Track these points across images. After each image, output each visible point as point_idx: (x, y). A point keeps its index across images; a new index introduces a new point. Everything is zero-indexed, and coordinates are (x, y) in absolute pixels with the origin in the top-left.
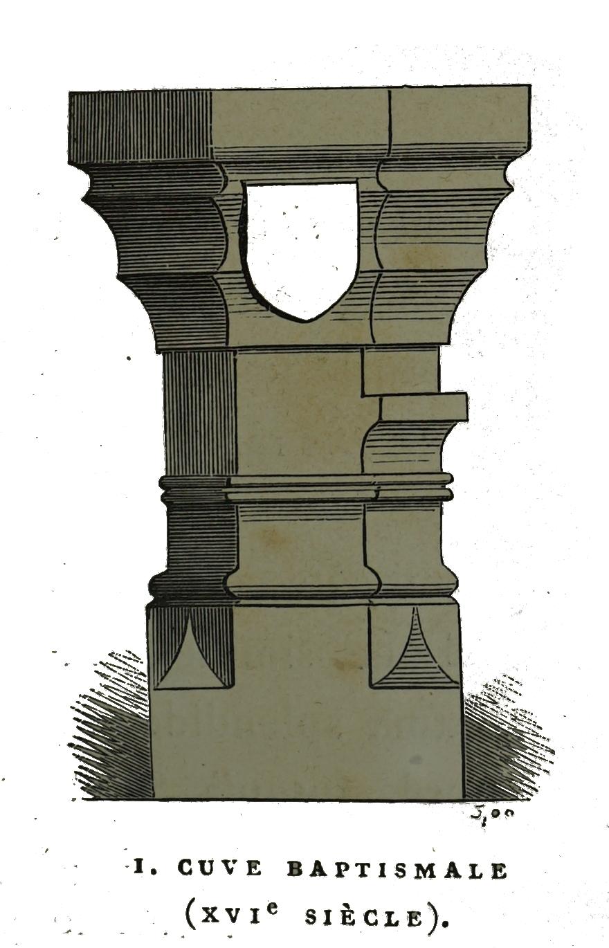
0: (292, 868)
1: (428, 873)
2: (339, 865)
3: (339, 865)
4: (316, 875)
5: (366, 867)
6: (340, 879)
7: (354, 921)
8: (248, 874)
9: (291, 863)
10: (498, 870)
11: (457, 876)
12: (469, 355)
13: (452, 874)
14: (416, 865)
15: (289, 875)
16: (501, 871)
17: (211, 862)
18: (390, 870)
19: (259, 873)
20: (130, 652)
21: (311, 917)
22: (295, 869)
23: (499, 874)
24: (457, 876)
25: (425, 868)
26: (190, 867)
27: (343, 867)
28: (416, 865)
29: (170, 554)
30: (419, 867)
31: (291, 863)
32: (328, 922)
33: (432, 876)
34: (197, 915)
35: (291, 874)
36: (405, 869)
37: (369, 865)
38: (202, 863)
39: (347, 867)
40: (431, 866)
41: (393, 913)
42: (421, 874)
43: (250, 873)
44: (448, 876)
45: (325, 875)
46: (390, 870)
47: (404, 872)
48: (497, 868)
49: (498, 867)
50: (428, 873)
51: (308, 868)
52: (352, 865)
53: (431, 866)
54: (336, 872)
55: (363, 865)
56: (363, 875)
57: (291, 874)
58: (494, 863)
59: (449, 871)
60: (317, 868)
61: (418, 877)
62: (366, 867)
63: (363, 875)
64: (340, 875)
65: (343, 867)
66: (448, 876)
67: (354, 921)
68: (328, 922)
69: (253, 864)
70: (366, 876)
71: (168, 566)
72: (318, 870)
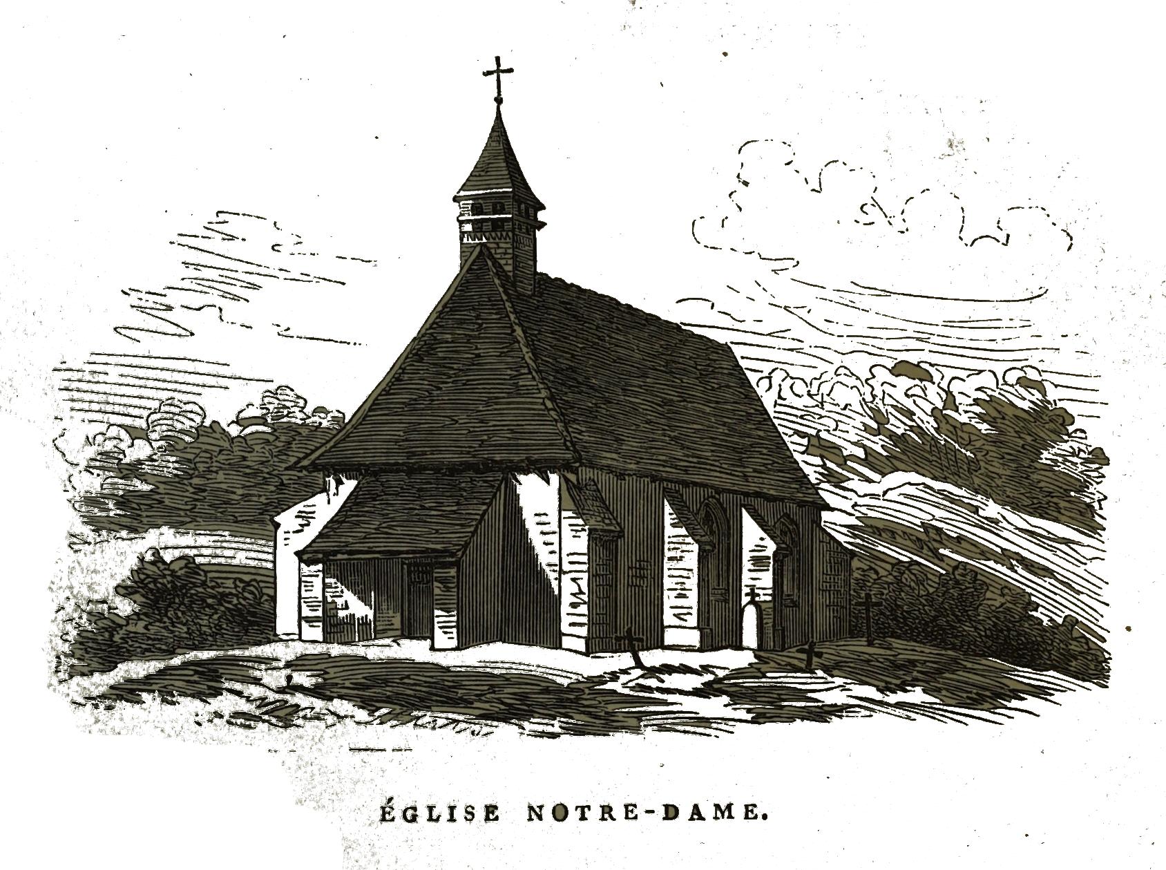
1: (726, 814)
4: (694, 819)
5: (586, 809)
6: (531, 822)
7: (636, 815)
9: (603, 807)
10: (957, 97)
11: (701, 818)
12: (903, 212)
13: (695, 817)
14: (715, 805)
15: (664, 819)
18: (459, 814)
20: (480, 662)
22: (535, 813)
23: (491, 817)
24: (701, 818)
25: (723, 808)
28: (715, 805)
29: (645, 647)
31: (603, 807)
33: (730, 817)
36: (474, 811)
37: (589, 807)
40: (729, 807)
42: (719, 814)
44: (692, 819)
45: (704, 819)
46: (480, 813)
47: (473, 815)
48: (957, 97)
50: (726, 814)
51: (685, 812)
53: (729, 807)
55: (583, 808)
56: (583, 818)
58: (545, 227)
59: (693, 814)
60: (695, 812)
61: (716, 818)
63: (583, 818)
66: (692, 819)
67: (636, 815)
70: (586, 819)
71: (625, 651)
72: (697, 813)
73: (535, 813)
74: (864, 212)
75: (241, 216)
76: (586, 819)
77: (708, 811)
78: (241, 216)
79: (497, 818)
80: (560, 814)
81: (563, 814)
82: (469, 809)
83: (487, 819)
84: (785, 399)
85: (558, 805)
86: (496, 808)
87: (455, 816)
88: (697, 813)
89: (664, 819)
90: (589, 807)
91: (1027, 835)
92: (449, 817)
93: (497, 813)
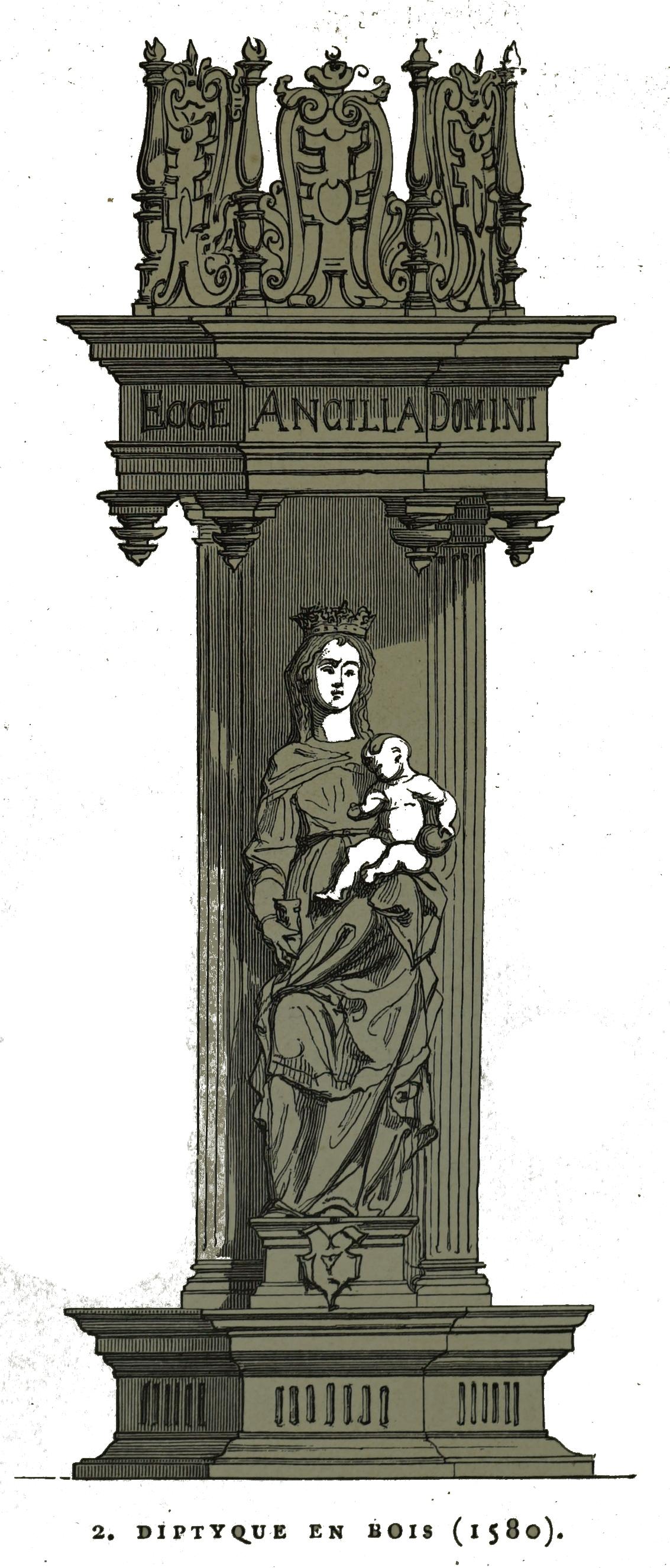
0: (141, 1532)
2: (176, 1528)
3: (176, 1528)
5: (200, 1529)
7: (321, 1534)
8: (411, 1537)
15: (139, 1538)
16: (317, 1531)
17: (263, 1527)
18: (419, 1532)
19: (320, 1536)
21: (428, 1532)
22: (336, 1532)
23: (316, 1534)
26: (502, 427)
27: (180, 1530)
30: (332, 1528)
32: (162, 1537)
34: (465, 1531)
35: (371, 1536)
36: (424, 1533)
37: (202, 1528)
38: (255, 1528)
39: (184, 1530)
41: (195, 1538)
43: (312, 1536)
46: (419, 1532)
47: (425, 1530)
49: (279, 1529)
51: (226, 1533)
52: (345, 430)
54: (174, 1535)
55: (198, 1528)
56: (198, 1537)
57: (371, 1536)
62: (200, 1529)
63: (198, 1537)
64: (177, 1537)
65: (180, 1530)
67: (321, 1534)
68: (162, 1537)
69: (315, 1528)
72: (217, 1530)
73: (279, 1531)
74: (336, 47)
75: (58, 1479)
76: (201, 1537)
77: (208, 1533)
78: (58, 1479)
79: (284, 1536)
80: (395, 1531)
81: (398, 1532)
82: (427, 1528)
83: (276, 1537)
84: (341, 661)
85: (394, 1524)
86: (283, 1527)
87: (416, 1534)
88: (217, 1530)
89: (139, 1538)
90: (202, 1528)
91: (449, 1493)
92: (139, 1535)
93: (320, 1531)
